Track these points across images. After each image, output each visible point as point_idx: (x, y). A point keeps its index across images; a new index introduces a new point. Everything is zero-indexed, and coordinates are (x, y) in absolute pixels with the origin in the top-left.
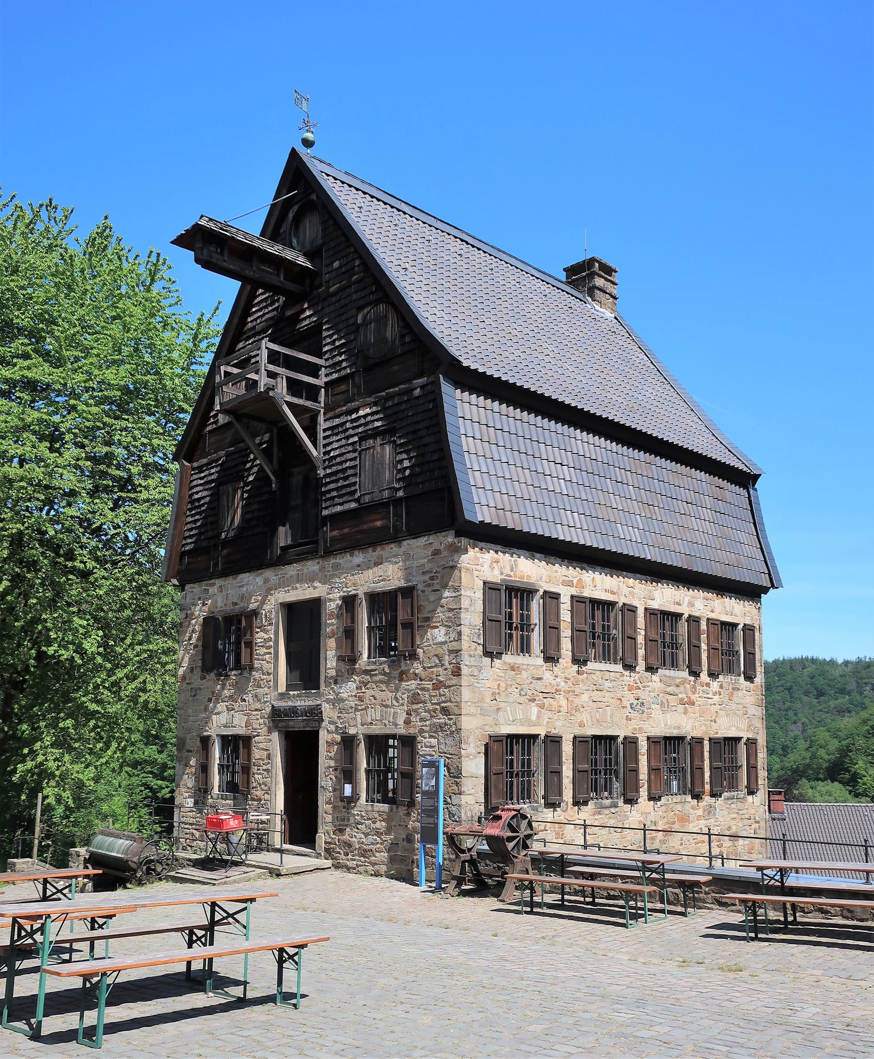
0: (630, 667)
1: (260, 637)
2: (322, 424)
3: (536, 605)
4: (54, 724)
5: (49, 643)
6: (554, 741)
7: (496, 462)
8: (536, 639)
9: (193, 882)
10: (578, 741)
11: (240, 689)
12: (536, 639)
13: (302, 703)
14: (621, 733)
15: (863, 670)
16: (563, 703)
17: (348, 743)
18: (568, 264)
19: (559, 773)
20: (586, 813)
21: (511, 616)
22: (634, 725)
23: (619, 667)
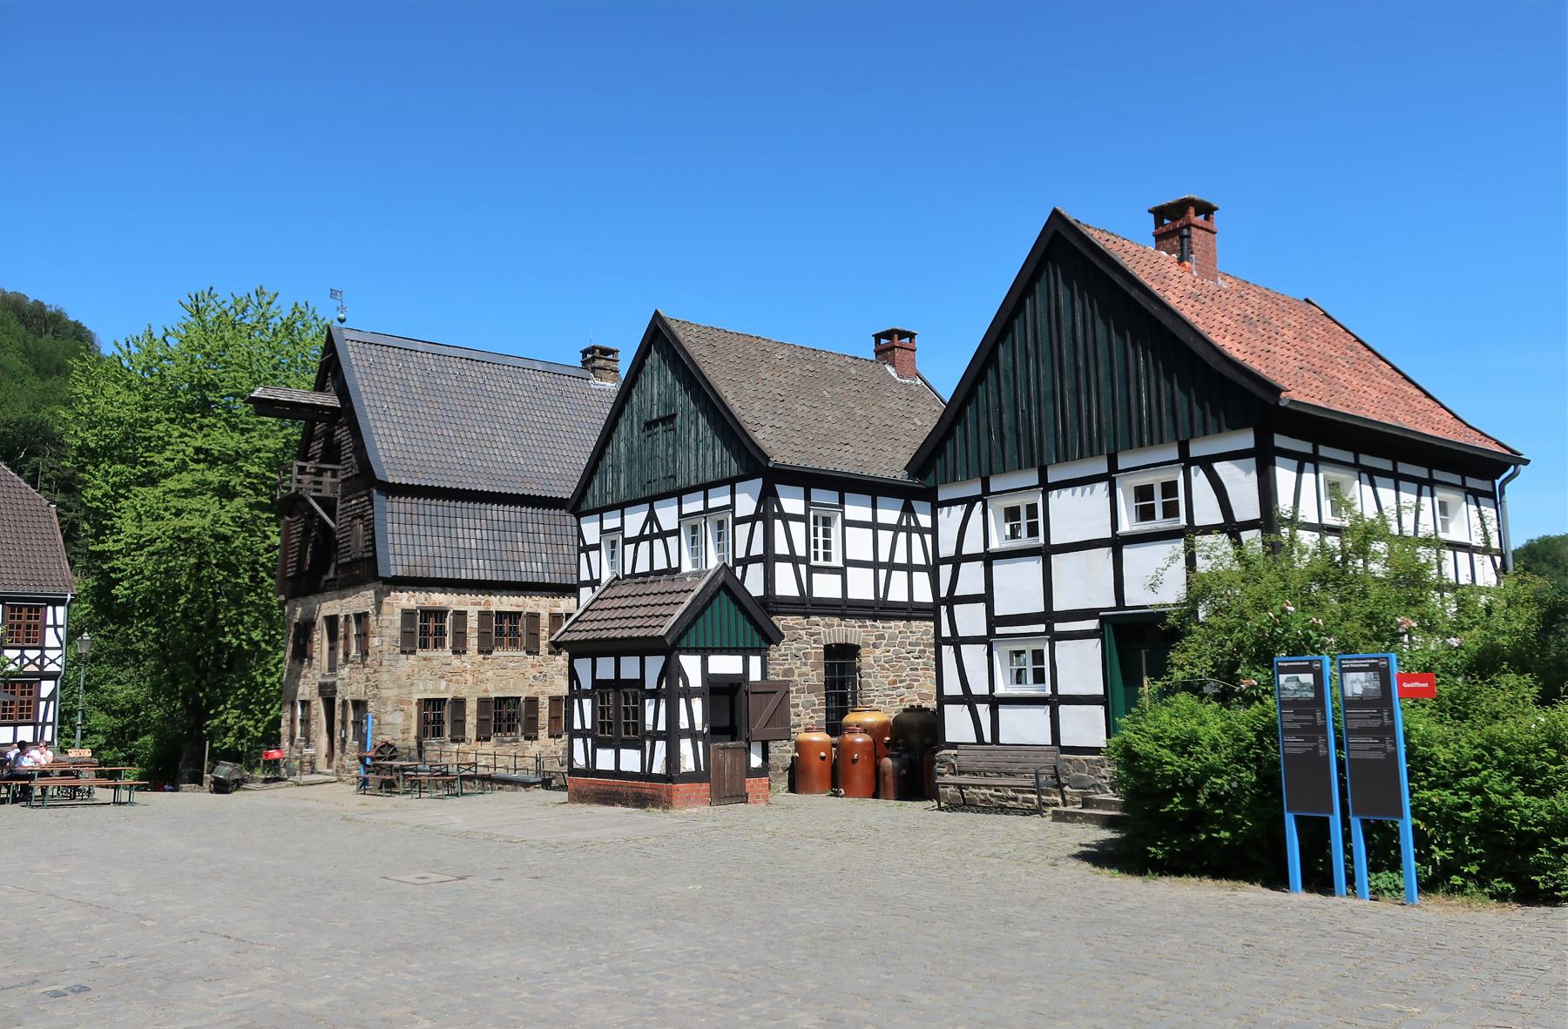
0: (533, 651)
1: (316, 637)
2: (339, 506)
3: (449, 619)
4: (264, 683)
5: (224, 635)
6: (459, 703)
7: (405, 538)
8: (448, 640)
9: (490, 781)
10: (483, 703)
11: (310, 665)
12: (448, 640)
13: (330, 680)
14: (523, 696)
15: (1561, 538)
16: (470, 678)
17: (344, 703)
18: (1071, 213)
19: (463, 722)
20: (487, 747)
21: (425, 630)
22: (536, 689)
23: (524, 653)
